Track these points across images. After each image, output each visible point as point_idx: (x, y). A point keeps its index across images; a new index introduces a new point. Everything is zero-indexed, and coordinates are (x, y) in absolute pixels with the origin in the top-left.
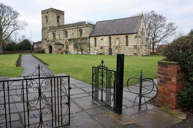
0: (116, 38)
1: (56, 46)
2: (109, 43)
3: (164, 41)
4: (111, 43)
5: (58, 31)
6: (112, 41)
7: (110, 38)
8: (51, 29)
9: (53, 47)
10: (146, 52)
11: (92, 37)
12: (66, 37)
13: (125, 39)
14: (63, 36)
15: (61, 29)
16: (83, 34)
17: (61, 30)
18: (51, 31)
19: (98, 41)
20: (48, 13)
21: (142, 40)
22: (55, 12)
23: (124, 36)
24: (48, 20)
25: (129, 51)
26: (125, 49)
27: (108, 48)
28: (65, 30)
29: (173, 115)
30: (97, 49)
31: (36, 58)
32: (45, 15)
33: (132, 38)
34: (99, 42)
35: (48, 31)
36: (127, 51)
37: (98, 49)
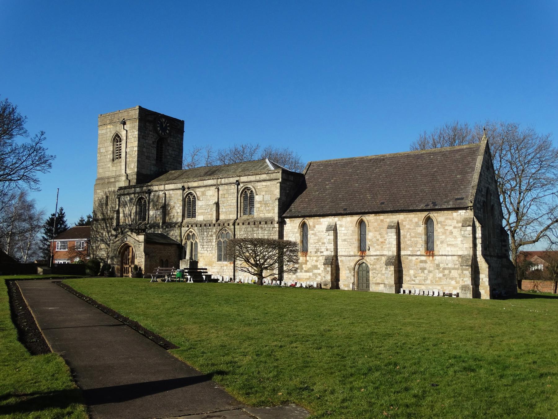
0: (386, 225)
2: (356, 244)
3: (12, 331)
4: (368, 243)
6: (370, 236)
13: (421, 229)
16: (256, 205)
19: (315, 234)
20: (124, 123)
23: (418, 218)
24: (123, 150)
26: (423, 269)
27: (352, 264)
28: (189, 188)
29: (378, 259)
30: (309, 265)
31: (70, 290)
33: (451, 228)
34: (319, 240)
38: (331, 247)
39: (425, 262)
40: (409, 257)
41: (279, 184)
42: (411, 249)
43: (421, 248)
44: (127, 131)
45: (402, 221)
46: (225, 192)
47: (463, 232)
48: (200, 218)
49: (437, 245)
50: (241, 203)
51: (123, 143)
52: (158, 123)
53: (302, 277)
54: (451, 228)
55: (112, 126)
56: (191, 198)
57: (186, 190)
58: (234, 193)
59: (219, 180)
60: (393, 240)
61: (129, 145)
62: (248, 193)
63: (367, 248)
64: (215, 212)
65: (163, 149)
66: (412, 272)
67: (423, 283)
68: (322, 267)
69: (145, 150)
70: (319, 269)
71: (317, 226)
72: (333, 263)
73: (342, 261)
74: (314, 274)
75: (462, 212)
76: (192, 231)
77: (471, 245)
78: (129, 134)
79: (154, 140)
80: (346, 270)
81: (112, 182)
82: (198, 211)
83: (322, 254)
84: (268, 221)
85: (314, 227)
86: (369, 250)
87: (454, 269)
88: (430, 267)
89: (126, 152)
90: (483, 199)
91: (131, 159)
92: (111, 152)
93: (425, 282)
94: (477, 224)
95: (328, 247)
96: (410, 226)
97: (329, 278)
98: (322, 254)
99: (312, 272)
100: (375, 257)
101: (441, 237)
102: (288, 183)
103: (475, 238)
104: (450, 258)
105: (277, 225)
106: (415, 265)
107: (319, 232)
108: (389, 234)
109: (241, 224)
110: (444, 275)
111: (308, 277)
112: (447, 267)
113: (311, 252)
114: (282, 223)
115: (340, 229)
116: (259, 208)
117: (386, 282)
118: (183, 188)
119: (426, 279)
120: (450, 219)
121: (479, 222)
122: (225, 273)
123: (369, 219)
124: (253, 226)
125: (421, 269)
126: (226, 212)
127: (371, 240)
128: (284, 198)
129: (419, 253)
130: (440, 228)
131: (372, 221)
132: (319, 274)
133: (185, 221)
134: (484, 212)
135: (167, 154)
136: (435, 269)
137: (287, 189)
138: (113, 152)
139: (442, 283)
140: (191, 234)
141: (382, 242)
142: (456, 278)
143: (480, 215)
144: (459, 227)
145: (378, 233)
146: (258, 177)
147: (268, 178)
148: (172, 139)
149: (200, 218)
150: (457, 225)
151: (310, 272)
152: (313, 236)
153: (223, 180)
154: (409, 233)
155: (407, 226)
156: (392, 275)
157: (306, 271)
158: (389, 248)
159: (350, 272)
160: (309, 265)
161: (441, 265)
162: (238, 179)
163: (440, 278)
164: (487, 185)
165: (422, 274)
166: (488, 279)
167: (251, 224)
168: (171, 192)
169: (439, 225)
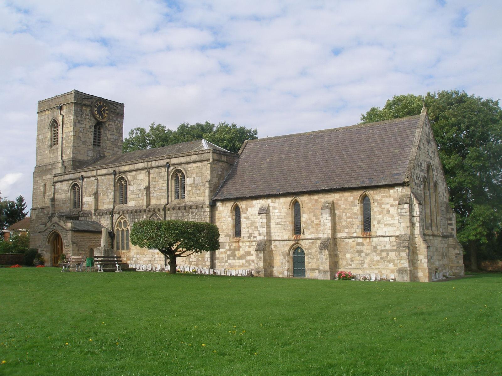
0: (320, 206)
1: (80, 235)
5: (93, 179)
6: (304, 218)
7: (296, 207)
8: (70, 169)
9: (64, 241)
10: (445, 261)
11: (223, 201)
12: (177, 197)
13: (357, 209)
14: (111, 196)
15: (104, 171)
16: (188, 188)
17: (105, 175)
18: (67, 177)
19: (247, 218)
20: (61, 108)
21: (428, 211)
23: (353, 197)
25: (378, 258)
26: (360, 252)
27: (287, 249)
28: (120, 173)
29: (313, 243)
30: (242, 252)
32: (48, 116)
33: (387, 206)
34: (252, 224)
35: (56, 179)
36: (367, 261)
37: (249, 253)
38: (264, 230)
39: (362, 244)
40: (345, 240)
41: (209, 165)
42: (347, 230)
43: (357, 229)
44: (63, 116)
45: (338, 200)
46: (156, 175)
47: (399, 211)
48: (131, 204)
49: (374, 226)
50: (171, 186)
51: (60, 127)
52: (96, 107)
53: (235, 264)
54: (387, 206)
55: (50, 112)
56: (123, 182)
57: (118, 175)
58: (164, 176)
59: (150, 163)
60: (327, 221)
61: (65, 131)
62: (179, 175)
63: (302, 231)
64: (145, 197)
65: (102, 133)
66: (348, 256)
67: (361, 267)
68: (253, 252)
69: (81, 135)
70: (252, 255)
71: (249, 209)
72: (265, 248)
73: (275, 246)
74: (247, 261)
75: (399, 189)
76: (124, 217)
77: (408, 224)
78: (66, 119)
79: (91, 124)
80: (280, 255)
81: (49, 169)
82: (130, 196)
83: (255, 239)
84: (199, 206)
85: (247, 210)
86: (303, 233)
87: (392, 251)
88: (367, 249)
89: (62, 138)
90: (422, 174)
91: (67, 145)
92: (48, 139)
93: (362, 266)
94: (415, 201)
95: (261, 232)
96: (346, 206)
97: (261, 264)
98: (255, 239)
99: (245, 258)
100: (310, 241)
101: (377, 217)
102: (220, 164)
103: (412, 217)
104: (387, 239)
105: (207, 210)
106: (351, 247)
107: (252, 215)
108: (324, 215)
109: (171, 209)
110: (382, 258)
111: (241, 264)
112: (384, 248)
113: (244, 237)
114: (213, 206)
115: (274, 211)
116: (190, 191)
117: (321, 268)
118: (115, 173)
119: (363, 263)
120: (387, 197)
121: (416, 198)
122: (156, 262)
123: (303, 200)
124: (184, 211)
125: (358, 252)
126: (157, 197)
127: (305, 222)
128: (215, 180)
129: (355, 235)
130: (376, 207)
131: (306, 202)
132: (253, 261)
133: (117, 207)
134: (424, 188)
135: (106, 138)
136: (372, 252)
137: (220, 170)
138: (51, 139)
139: (380, 267)
140: (122, 220)
141: (317, 224)
142: (394, 260)
143: (419, 192)
144: (396, 205)
145: (312, 215)
146: (188, 159)
147: (198, 159)
148: (111, 123)
149: (131, 204)
150: (394, 203)
151: (235, 260)
152: (245, 220)
153: (153, 163)
154: (344, 214)
155: (343, 206)
156: (326, 259)
157: (239, 258)
158: (324, 230)
159: (285, 258)
160: (242, 252)
161: (379, 247)
162: (168, 161)
163: (378, 262)
164: (428, 160)
165: (359, 258)
166: (426, 261)
167: (182, 208)
168: (103, 177)
169: (376, 204)
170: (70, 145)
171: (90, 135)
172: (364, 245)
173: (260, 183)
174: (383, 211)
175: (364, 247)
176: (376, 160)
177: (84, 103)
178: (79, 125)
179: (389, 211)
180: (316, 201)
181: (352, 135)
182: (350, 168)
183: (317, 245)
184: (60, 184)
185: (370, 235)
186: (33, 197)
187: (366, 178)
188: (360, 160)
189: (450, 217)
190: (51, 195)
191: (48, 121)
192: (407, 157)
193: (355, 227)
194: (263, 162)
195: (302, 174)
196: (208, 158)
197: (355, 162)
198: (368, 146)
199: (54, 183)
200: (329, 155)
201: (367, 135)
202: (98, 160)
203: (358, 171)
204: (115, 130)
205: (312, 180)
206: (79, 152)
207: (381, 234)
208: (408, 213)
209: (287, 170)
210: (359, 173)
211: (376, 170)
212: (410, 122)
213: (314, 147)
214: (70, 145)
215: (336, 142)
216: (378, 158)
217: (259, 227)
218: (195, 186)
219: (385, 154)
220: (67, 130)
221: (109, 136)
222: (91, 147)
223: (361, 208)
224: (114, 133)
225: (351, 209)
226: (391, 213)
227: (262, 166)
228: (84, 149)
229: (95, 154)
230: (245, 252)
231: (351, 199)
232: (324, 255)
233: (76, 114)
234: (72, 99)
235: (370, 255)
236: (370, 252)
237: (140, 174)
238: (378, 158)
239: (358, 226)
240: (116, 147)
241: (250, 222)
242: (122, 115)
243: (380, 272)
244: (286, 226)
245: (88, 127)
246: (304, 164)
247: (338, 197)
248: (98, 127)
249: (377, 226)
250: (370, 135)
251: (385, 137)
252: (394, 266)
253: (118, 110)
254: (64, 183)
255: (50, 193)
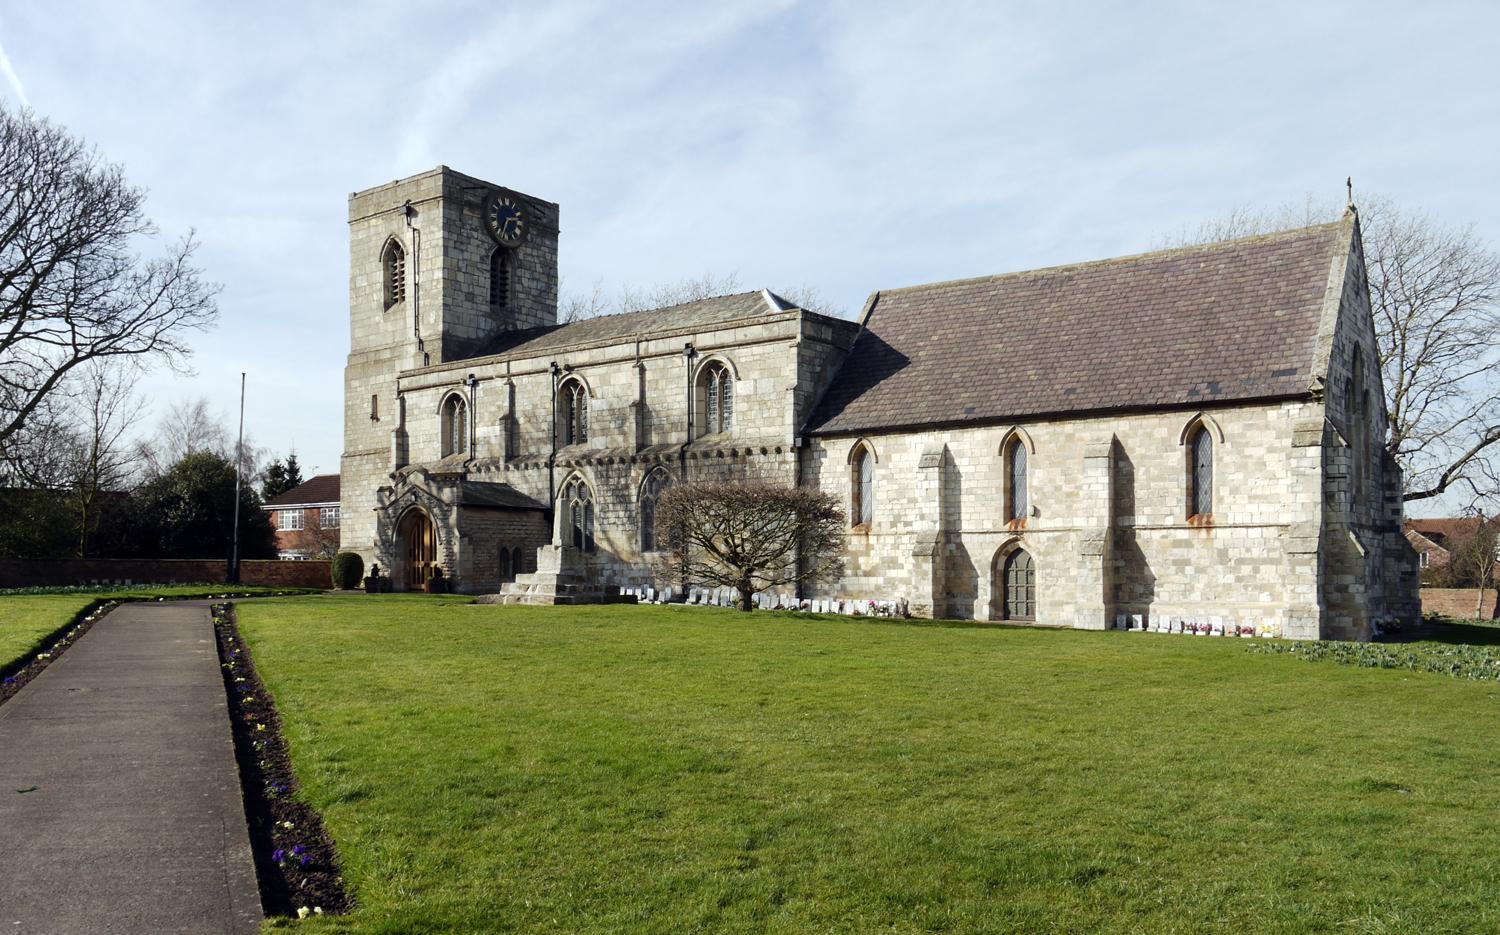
8: (436, 358)
13: (1178, 456)
18: (432, 378)
19: (889, 478)
20: (410, 212)
22: (471, 205)
25: (1230, 578)
28: (569, 368)
29: (1057, 540)
33: (1261, 451)
34: (902, 492)
36: (1200, 585)
39: (1188, 544)
41: (795, 350)
51: (409, 261)
52: (494, 211)
55: (380, 221)
60: (1100, 487)
69: (461, 277)
70: (901, 567)
71: (895, 457)
75: (1294, 408)
79: (484, 253)
83: (909, 529)
85: (888, 458)
88: (1200, 557)
91: (428, 301)
93: (1185, 597)
95: (925, 511)
98: (909, 529)
100: (1050, 534)
101: (1231, 477)
102: (819, 348)
104: (1254, 533)
105: (791, 457)
107: (901, 471)
110: (1239, 579)
112: (1248, 556)
113: (880, 524)
116: (744, 413)
119: (1188, 590)
120: (1259, 428)
125: (1175, 562)
127: (1038, 490)
128: (808, 387)
129: (1169, 521)
130: (1228, 453)
137: (817, 361)
141: (1069, 495)
144: (1282, 449)
145: (1057, 470)
148: (529, 251)
149: (597, 443)
152: (884, 482)
156: (1096, 580)
161: (1231, 553)
162: (689, 339)
163: (1228, 587)
164: (1356, 338)
165: (1178, 578)
168: (525, 379)
170: (436, 302)
171: (482, 279)
172: (1192, 546)
173: (921, 394)
174: (1246, 464)
175: (1192, 550)
176: (1225, 337)
177: (468, 200)
178: (453, 253)
179: (1264, 464)
180: (1070, 437)
181: (1151, 276)
182: (1155, 356)
183: (1070, 544)
184: (415, 394)
185: (1208, 522)
186: (346, 426)
187: (1200, 380)
188: (1180, 336)
189: (1390, 480)
190: (394, 420)
191: (378, 243)
192: (1310, 329)
193: (1171, 501)
194: (921, 344)
195: (1029, 373)
196: (790, 333)
197: (1168, 343)
198: (1197, 302)
199: (399, 392)
200: (1094, 325)
201: (1194, 276)
202: (504, 340)
203: (1177, 364)
204: (539, 268)
205: (1057, 387)
206: (458, 318)
207: (1238, 521)
208: (1319, 470)
209: (987, 362)
210: (1181, 370)
211: (1225, 362)
212: (1308, 242)
213: (1053, 305)
214: (436, 302)
215: (1110, 293)
216: (1229, 331)
217: (920, 500)
218: (757, 400)
219: (1248, 323)
220: (427, 270)
221: (525, 282)
222: (486, 308)
223: (1187, 454)
224: (536, 275)
225: (1161, 457)
226: (1268, 468)
227: (921, 354)
228: (471, 312)
229: (494, 324)
230: (882, 558)
231: (1163, 432)
232: (1092, 570)
233: (447, 226)
234: (436, 187)
235: (1209, 570)
236: (1207, 564)
237: (619, 370)
238: (1229, 331)
239: (1179, 501)
240: (542, 310)
241: (896, 487)
242: (551, 231)
243: (1234, 611)
244: (989, 497)
245: (476, 258)
246: (1031, 347)
247: (1127, 427)
248: (500, 261)
249: (1228, 499)
250: (1200, 275)
251: (1243, 280)
252: (1273, 600)
253: (545, 221)
254: (424, 392)
255: (389, 418)
